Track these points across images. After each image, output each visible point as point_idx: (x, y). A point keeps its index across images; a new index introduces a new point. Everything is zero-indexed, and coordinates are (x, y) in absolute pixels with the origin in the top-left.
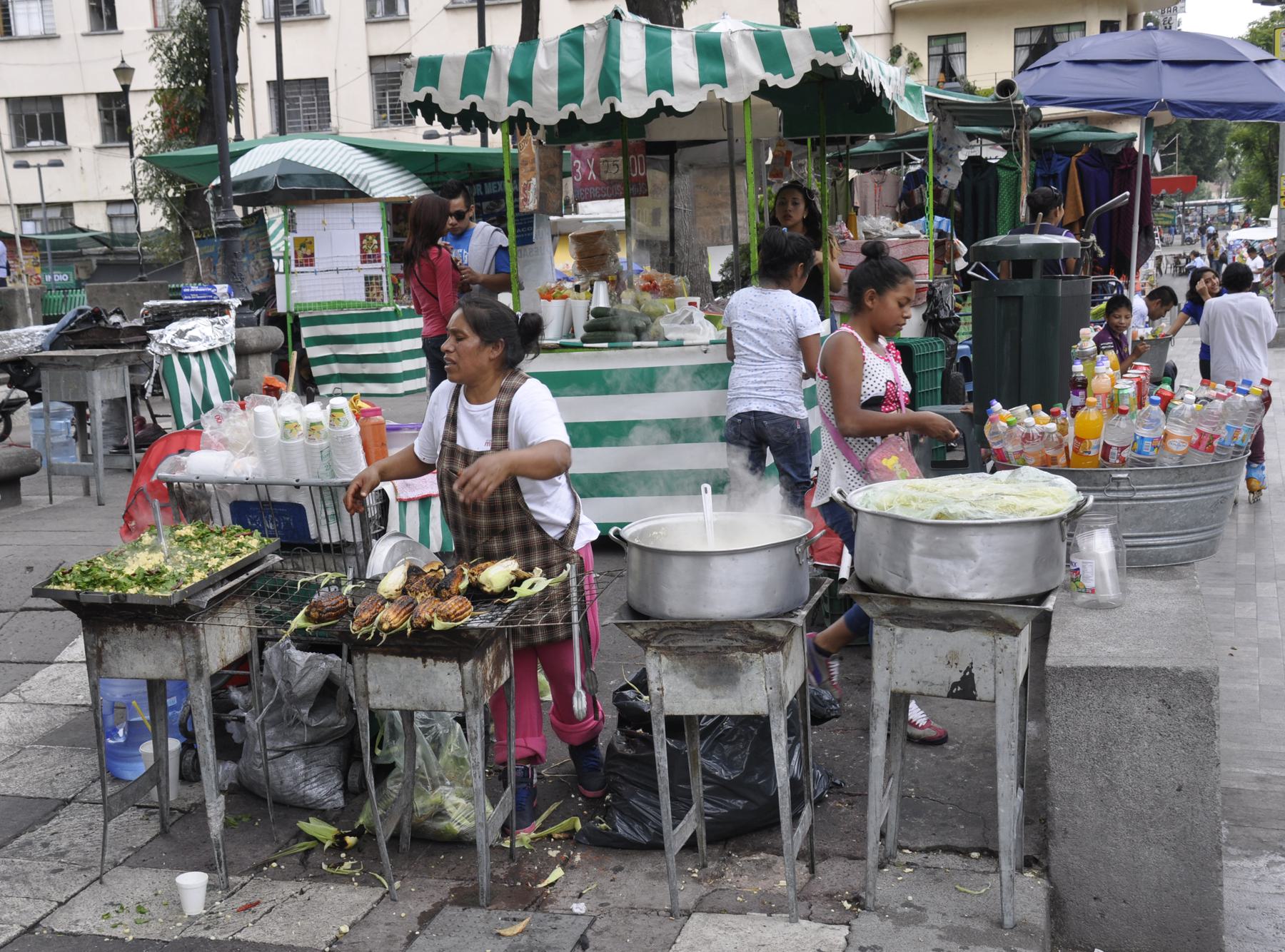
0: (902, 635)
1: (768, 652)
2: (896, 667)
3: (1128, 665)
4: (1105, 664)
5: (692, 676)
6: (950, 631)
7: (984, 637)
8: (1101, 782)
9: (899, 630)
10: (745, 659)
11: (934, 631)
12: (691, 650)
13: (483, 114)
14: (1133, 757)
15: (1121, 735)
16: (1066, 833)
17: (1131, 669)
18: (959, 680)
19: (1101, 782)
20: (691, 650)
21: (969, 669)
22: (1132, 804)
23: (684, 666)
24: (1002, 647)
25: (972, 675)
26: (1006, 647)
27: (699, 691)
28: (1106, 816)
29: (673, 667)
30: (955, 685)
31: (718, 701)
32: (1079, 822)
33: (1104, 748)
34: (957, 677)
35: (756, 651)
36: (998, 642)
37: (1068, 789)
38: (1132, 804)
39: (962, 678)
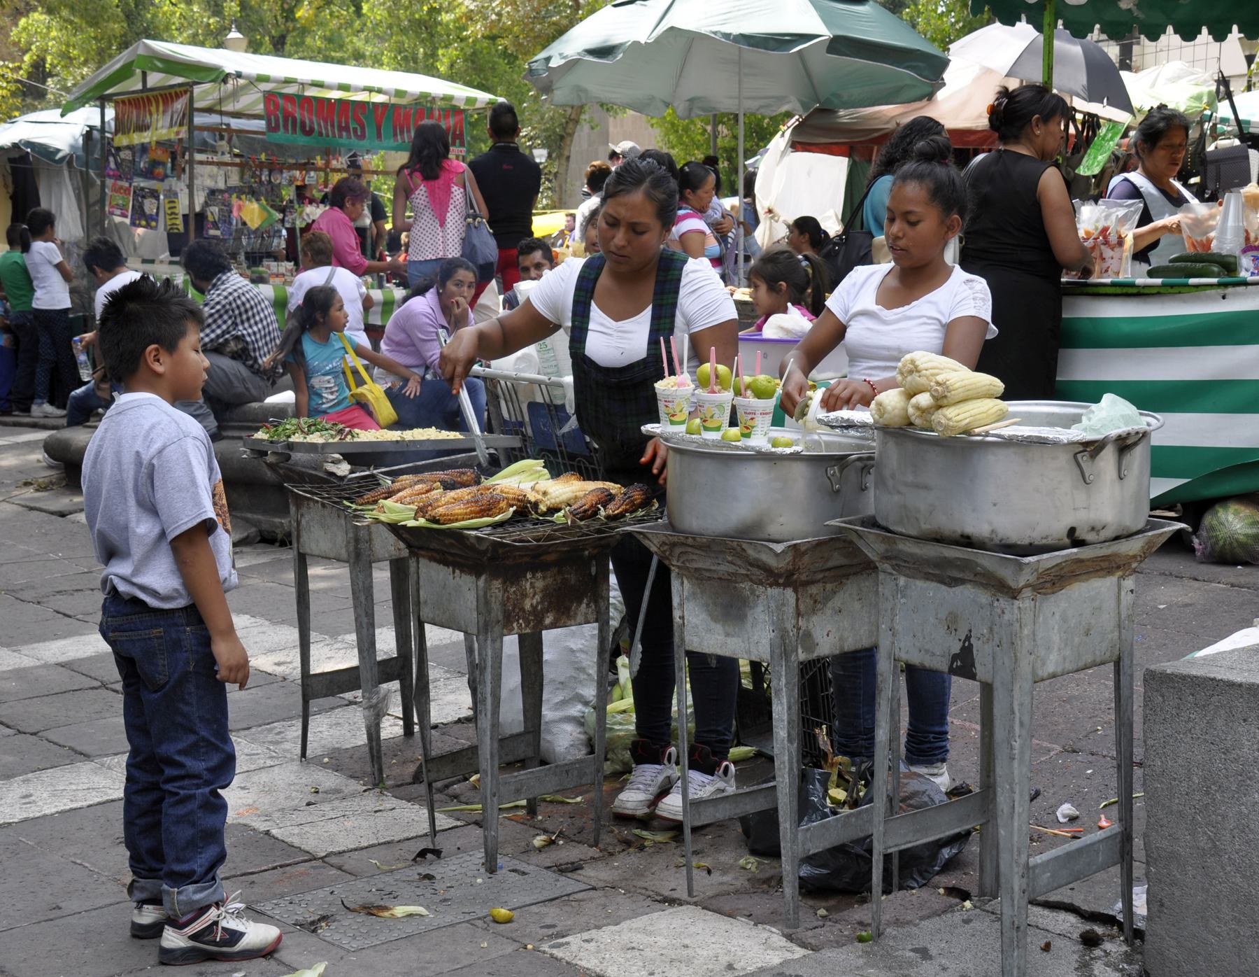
0: (906, 587)
1: (771, 586)
2: (898, 627)
3: (1239, 679)
4: (1212, 676)
5: (708, 605)
6: (950, 585)
7: (984, 597)
8: (1203, 842)
9: (902, 581)
10: (753, 592)
11: (934, 584)
12: (708, 574)
13: (1013, 25)
14: (1240, 813)
15: (1227, 777)
16: (1162, 905)
17: (1240, 685)
18: (958, 651)
19: (1203, 842)
20: (708, 574)
21: (968, 638)
22: (1239, 880)
23: (702, 593)
24: (999, 611)
25: (971, 645)
26: (1003, 612)
27: (713, 625)
28: (1208, 891)
29: (694, 593)
30: (955, 657)
31: (729, 640)
32: (1177, 893)
33: (1207, 793)
34: (956, 648)
35: (760, 583)
36: (996, 604)
37: (1165, 844)
38: (1239, 880)
39: (961, 649)
